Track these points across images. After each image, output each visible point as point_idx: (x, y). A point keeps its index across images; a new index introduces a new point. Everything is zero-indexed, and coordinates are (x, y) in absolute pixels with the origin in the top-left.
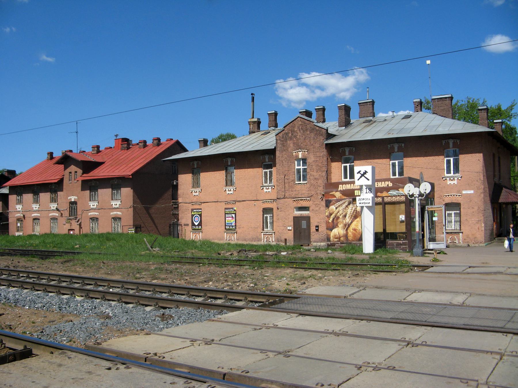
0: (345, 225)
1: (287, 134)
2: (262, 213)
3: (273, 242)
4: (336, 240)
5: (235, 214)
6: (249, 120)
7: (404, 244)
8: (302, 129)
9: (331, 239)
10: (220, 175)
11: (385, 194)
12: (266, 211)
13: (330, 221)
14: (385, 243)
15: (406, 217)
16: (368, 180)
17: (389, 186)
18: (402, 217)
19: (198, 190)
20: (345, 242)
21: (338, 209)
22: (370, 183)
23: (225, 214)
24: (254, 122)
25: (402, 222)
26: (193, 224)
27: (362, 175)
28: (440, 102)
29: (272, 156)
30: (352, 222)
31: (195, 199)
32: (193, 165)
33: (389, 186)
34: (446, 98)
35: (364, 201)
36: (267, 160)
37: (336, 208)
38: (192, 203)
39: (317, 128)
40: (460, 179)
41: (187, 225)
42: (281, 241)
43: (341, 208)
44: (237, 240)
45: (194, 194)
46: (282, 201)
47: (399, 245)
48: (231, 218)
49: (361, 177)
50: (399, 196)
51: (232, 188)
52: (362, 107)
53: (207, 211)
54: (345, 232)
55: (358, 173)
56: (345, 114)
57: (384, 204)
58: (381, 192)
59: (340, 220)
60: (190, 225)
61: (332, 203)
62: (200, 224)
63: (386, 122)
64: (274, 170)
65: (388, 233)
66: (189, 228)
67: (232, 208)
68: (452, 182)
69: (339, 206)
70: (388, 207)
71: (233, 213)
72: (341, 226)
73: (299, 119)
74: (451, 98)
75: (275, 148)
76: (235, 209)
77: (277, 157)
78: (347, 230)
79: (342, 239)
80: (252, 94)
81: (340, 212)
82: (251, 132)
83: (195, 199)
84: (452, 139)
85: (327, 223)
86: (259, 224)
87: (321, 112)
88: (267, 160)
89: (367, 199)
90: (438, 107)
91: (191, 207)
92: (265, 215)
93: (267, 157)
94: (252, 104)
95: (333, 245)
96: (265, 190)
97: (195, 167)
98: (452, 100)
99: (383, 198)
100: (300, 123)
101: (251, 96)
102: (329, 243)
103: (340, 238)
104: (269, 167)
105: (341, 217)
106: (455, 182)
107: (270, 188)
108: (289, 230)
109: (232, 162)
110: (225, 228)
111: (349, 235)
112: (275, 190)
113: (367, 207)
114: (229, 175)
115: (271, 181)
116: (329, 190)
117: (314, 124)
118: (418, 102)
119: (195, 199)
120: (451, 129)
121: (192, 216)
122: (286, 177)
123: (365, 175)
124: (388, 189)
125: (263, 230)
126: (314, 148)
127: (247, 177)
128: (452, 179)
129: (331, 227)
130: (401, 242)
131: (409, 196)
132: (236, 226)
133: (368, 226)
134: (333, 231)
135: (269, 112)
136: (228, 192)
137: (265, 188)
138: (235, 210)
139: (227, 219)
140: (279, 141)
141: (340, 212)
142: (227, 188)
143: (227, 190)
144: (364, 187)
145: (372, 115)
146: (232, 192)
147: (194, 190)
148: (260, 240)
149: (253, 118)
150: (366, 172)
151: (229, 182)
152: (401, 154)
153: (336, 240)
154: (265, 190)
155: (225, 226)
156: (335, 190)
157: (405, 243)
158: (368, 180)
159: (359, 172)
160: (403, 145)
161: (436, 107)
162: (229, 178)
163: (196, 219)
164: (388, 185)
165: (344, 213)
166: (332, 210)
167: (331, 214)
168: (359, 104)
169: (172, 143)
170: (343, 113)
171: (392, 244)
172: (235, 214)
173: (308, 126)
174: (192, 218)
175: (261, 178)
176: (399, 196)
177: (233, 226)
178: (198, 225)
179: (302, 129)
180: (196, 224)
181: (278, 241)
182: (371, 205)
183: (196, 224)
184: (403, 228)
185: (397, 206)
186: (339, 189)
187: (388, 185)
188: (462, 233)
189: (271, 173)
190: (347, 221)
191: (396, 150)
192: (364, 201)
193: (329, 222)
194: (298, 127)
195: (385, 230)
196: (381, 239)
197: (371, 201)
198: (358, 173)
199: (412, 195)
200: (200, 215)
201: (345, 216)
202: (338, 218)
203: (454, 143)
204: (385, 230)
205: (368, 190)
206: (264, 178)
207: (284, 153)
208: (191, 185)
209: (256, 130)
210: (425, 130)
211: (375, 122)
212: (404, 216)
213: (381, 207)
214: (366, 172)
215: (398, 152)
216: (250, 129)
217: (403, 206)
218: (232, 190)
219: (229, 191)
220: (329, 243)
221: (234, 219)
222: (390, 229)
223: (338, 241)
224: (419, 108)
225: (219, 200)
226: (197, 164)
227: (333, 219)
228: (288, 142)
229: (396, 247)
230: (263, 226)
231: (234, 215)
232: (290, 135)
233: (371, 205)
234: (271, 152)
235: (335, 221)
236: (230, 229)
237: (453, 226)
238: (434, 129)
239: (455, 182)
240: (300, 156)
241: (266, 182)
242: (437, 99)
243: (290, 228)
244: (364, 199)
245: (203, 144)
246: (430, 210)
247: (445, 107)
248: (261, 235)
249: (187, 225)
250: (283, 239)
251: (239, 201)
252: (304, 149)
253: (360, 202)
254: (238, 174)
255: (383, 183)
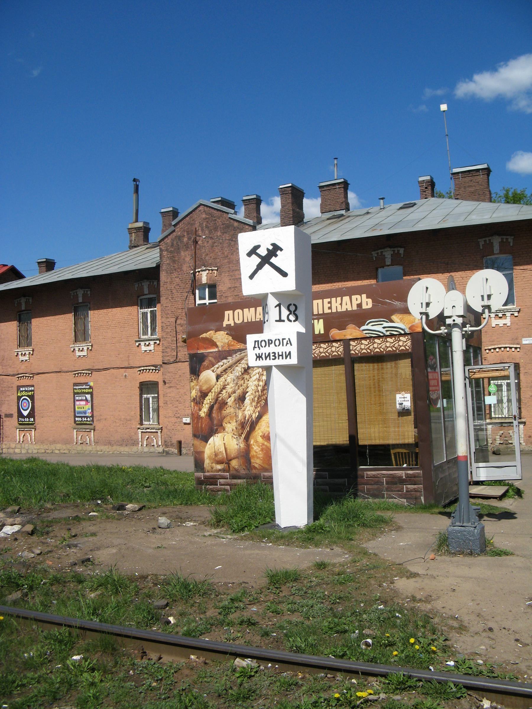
0: (242, 425)
1: (179, 238)
2: (138, 392)
3: (158, 446)
4: (219, 467)
5: (91, 394)
6: (130, 226)
7: (411, 480)
8: (207, 227)
9: (207, 463)
10: (64, 322)
11: (351, 332)
12: (147, 387)
13: (202, 414)
14: (356, 477)
15: (415, 399)
16: (284, 274)
17: (364, 307)
18: (404, 399)
19: (27, 350)
20: (243, 472)
21: (222, 379)
22: (289, 284)
23: (75, 394)
24: (138, 229)
25: (404, 413)
26: (20, 415)
27: (265, 260)
28: (468, 179)
29: (155, 283)
30: (260, 417)
31: (23, 367)
32: (20, 304)
33: (364, 307)
34: (478, 170)
35: (272, 349)
36: (146, 291)
37: (218, 377)
38: (19, 375)
39: (236, 224)
40: (516, 314)
41: (10, 416)
42: (172, 445)
43: (230, 377)
44: (96, 443)
45: (21, 358)
46: (171, 368)
47: (395, 482)
48: (83, 403)
49: (260, 267)
50: (392, 336)
51: (84, 346)
52: (327, 193)
53: (43, 387)
54: (242, 445)
55: (249, 254)
56: (293, 204)
57: (350, 362)
58: (342, 327)
59: (229, 410)
60: (16, 415)
61: (206, 363)
62: (32, 414)
63: (369, 216)
64: (158, 309)
65: (365, 446)
66: (14, 421)
67: (86, 384)
68: (501, 322)
69: (225, 370)
70: (362, 372)
71: (88, 393)
72: (230, 426)
73: (201, 208)
74: (488, 171)
75: (158, 267)
76: (92, 384)
77: (162, 284)
78: (247, 439)
79: (234, 463)
80: (135, 180)
81: (229, 389)
82: (132, 247)
83: (22, 368)
84: (499, 235)
85: (195, 417)
86: (133, 413)
87: (253, 206)
88: (146, 291)
89: (281, 342)
90: (465, 188)
91: (15, 382)
92: (145, 396)
93: (146, 286)
94: (134, 196)
95: (212, 480)
96: (143, 348)
97: (23, 308)
98: (488, 175)
99: (346, 343)
100: (204, 216)
101: (133, 183)
102: (201, 475)
103: (227, 461)
104: (151, 303)
105: (230, 401)
106: (508, 321)
107: (152, 342)
108: (185, 424)
109: (84, 296)
110: (75, 421)
111: (253, 453)
112: (160, 348)
113: (280, 368)
114: (80, 322)
115: (153, 330)
116: (198, 327)
117: (230, 216)
118: (427, 181)
119: (23, 367)
120: (494, 215)
121: (19, 398)
122: (179, 322)
123: (273, 260)
124: (359, 317)
125: (141, 424)
126: (229, 263)
127: (112, 323)
128: (500, 315)
129: (206, 430)
130: (402, 473)
131: (430, 323)
132: (92, 416)
133: (288, 439)
134: (211, 440)
135: (163, 210)
136: (78, 354)
137: (142, 343)
138: (91, 388)
139: (77, 403)
140: (165, 253)
141: (229, 389)
142: (77, 346)
143: (77, 349)
144: (272, 302)
145: (344, 206)
146: (84, 353)
147: (21, 350)
148: (135, 443)
149: (137, 221)
150: (275, 250)
151: (81, 334)
152: (399, 269)
153: (219, 467)
154: (143, 348)
155: (75, 416)
156: (213, 326)
157: (414, 476)
158: (284, 274)
159: (253, 252)
160: (402, 251)
161: (460, 188)
162: (80, 327)
163: (25, 404)
164: (360, 305)
165: (239, 392)
166: (207, 381)
167: (204, 395)
168: (321, 187)
169: (5, 268)
170: (290, 201)
171: (377, 481)
172: (91, 394)
173: (219, 222)
174: (18, 403)
175: (135, 325)
176: (392, 336)
177: (87, 417)
178: (29, 416)
179: (207, 227)
180: (25, 413)
181: (167, 446)
182: (294, 360)
183: (25, 413)
184: (406, 433)
185: (389, 366)
186: (224, 324)
187: (360, 305)
188: (524, 423)
189: (153, 314)
190: (247, 413)
191: (388, 261)
192: (272, 349)
193: (199, 417)
194: (201, 225)
195: (353, 438)
196: (337, 469)
197: (293, 349)
198: (249, 254)
199: (441, 318)
200: (32, 397)
201: (242, 399)
202: (223, 404)
203: (501, 243)
204: (353, 438)
205: (285, 312)
206: (141, 325)
207: (175, 274)
208: (16, 343)
209: (141, 242)
210: (443, 220)
211: (349, 217)
212: (408, 396)
213: (338, 372)
214: (275, 250)
215: (392, 265)
216: (131, 241)
217: (405, 367)
218: (85, 348)
219: (81, 350)
220: (201, 475)
221: (90, 404)
222: (370, 435)
223: (224, 470)
224: (429, 191)
225: (64, 369)
226: (26, 303)
227: (211, 408)
228: (182, 253)
229: (387, 490)
230: (141, 416)
231: (88, 397)
232: (185, 239)
233: (294, 360)
234: (151, 275)
235: (214, 415)
236: (84, 423)
237: (505, 411)
238: (462, 218)
239: (508, 321)
240: (204, 280)
241: (145, 333)
242: (462, 172)
243: (188, 420)
244: (270, 342)
245: (44, 269)
246: (477, 376)
247: (478, 188)
248: (136, 434)
249: (10, 416)
250: (175, 441)
251: (98, 370)
252: (210, 265)
253: (257, 351)
254: (97, 318)
255: (346, 299)
